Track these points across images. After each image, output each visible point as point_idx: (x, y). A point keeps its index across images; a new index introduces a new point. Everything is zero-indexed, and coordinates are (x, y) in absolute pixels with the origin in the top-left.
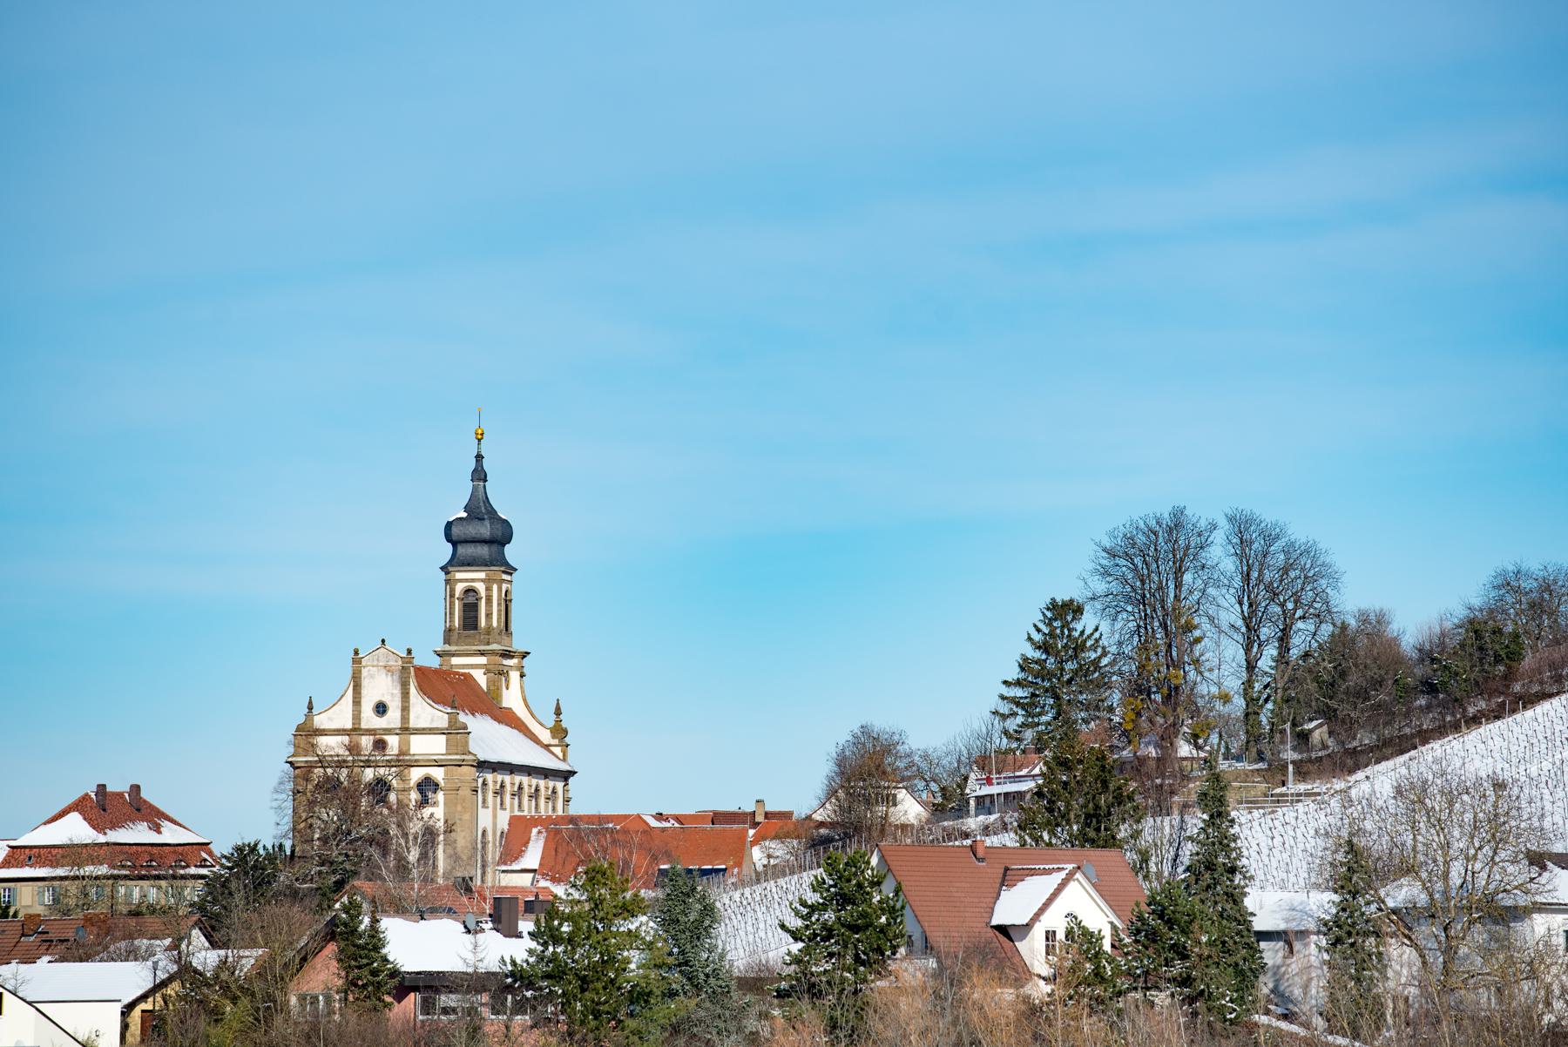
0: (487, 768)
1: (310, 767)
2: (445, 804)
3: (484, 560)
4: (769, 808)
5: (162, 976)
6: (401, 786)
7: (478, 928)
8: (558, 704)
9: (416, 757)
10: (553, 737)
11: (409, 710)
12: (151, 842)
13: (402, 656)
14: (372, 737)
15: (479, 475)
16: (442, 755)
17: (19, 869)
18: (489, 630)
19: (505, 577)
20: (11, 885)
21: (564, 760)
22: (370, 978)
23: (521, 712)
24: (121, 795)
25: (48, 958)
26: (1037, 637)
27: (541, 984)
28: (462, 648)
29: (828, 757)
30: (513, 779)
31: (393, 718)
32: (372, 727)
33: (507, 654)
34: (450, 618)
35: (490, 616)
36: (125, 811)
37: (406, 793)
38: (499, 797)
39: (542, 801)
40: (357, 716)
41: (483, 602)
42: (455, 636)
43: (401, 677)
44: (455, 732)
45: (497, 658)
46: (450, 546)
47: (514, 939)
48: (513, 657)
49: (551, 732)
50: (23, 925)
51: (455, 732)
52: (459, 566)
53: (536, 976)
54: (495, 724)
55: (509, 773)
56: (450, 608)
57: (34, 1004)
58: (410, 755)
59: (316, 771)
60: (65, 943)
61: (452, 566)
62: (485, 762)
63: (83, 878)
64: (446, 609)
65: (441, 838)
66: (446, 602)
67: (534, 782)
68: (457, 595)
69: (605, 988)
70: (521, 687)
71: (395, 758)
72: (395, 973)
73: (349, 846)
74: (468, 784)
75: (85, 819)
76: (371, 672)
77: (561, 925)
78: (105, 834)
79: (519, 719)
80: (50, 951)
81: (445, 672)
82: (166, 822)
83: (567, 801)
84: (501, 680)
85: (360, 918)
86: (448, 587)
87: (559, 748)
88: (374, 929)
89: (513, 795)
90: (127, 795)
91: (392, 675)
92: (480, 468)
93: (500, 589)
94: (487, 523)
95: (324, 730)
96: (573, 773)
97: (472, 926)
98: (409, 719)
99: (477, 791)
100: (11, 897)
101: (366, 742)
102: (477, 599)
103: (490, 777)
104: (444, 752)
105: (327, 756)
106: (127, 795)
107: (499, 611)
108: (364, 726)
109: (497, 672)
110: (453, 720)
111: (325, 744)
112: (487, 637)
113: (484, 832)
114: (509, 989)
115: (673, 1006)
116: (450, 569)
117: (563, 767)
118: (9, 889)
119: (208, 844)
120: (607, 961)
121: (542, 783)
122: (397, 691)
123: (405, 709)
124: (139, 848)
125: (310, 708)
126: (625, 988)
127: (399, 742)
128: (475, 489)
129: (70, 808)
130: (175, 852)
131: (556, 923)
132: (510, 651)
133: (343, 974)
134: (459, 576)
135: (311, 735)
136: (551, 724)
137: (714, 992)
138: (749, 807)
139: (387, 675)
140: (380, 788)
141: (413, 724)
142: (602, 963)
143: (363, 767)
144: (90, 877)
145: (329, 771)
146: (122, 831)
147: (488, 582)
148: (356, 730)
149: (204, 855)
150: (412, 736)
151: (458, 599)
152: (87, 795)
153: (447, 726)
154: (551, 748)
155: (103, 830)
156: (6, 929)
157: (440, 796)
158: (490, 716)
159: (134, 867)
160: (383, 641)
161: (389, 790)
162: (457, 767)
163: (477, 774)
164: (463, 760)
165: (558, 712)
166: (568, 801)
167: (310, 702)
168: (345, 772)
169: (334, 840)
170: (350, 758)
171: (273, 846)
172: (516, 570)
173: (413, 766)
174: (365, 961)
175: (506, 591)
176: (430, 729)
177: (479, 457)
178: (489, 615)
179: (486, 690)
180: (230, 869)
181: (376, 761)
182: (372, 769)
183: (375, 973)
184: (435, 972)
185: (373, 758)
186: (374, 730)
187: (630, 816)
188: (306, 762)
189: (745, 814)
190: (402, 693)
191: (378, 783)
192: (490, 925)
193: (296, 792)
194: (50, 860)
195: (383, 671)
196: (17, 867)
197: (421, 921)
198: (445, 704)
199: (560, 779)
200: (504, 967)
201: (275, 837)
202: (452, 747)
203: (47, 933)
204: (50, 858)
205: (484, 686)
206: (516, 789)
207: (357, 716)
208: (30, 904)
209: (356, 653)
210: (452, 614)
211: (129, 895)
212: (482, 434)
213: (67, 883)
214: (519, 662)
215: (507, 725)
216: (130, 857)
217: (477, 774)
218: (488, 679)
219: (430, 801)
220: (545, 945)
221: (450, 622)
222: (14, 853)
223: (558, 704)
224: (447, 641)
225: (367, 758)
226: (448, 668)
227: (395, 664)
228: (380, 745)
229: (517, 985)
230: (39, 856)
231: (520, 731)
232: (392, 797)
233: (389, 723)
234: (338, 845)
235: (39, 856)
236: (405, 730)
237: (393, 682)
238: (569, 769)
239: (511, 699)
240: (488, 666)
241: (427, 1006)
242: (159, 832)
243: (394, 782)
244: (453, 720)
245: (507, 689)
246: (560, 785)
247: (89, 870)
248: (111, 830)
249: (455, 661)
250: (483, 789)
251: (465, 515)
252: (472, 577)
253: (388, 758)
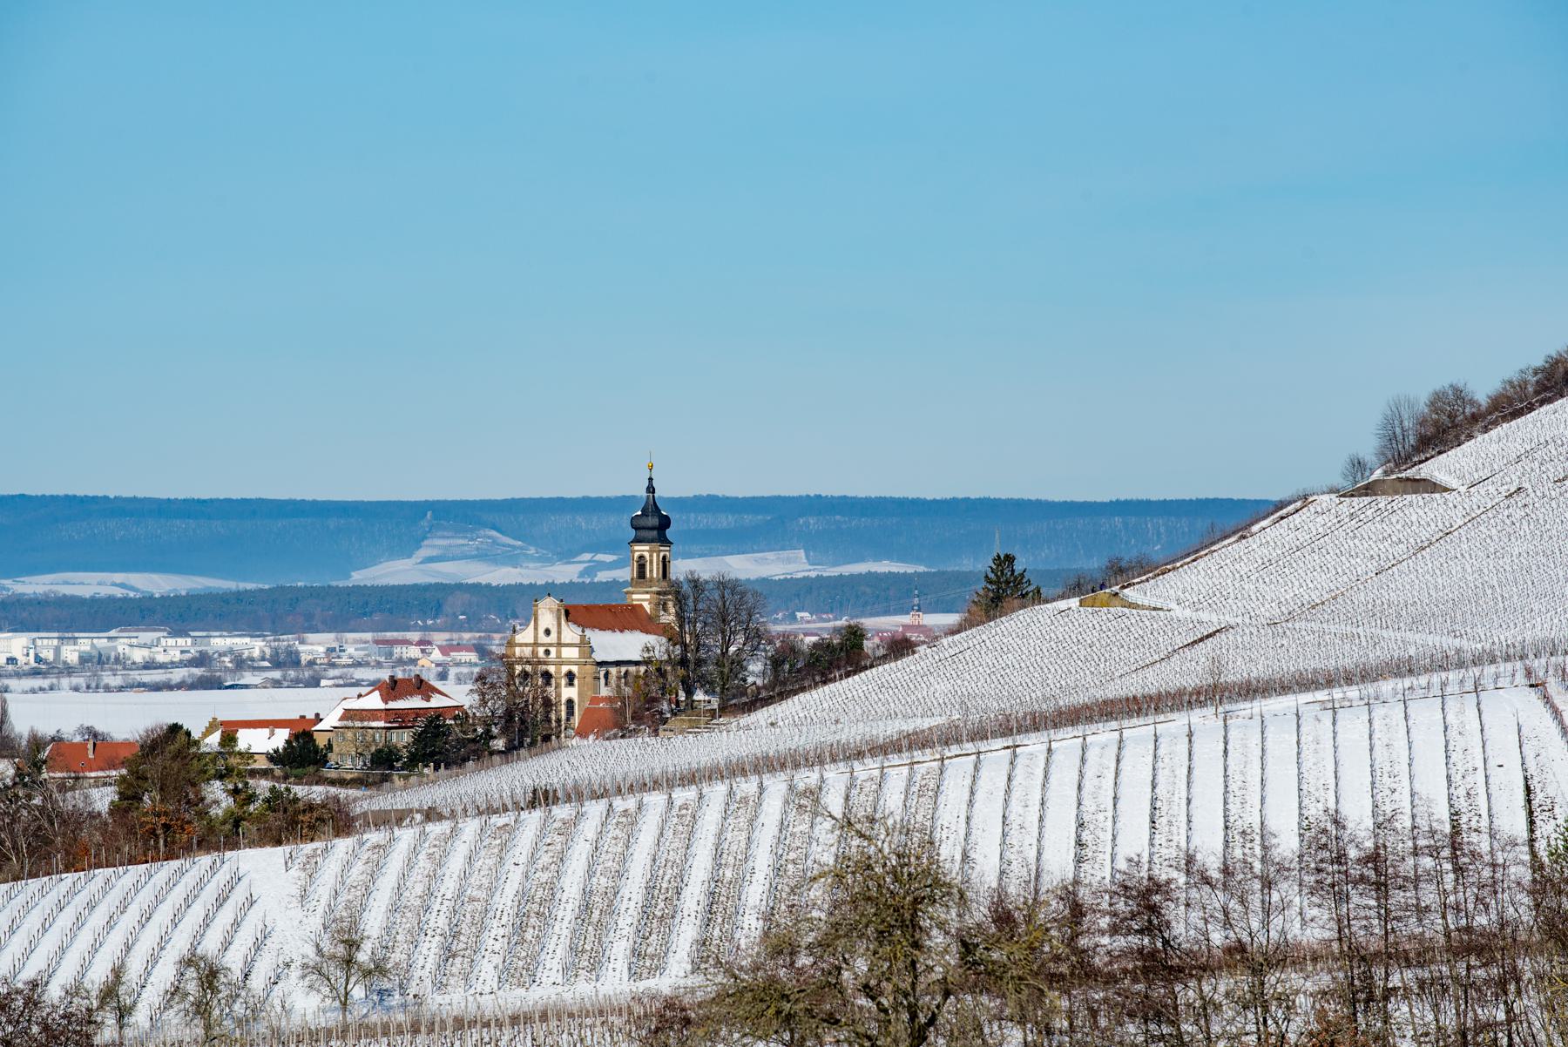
18: (652, 578)
26: (992, 576)
31: (553, 638)
40: (536, 637)
93: (658, 556)
101: (541, 651)
107: (658, 569)
122: (555, 623)
123: (559, 633)
134: (636, 548)
141: (563, 641)
147: (651, 552)
148: (536, 644)
159: (403, 721)
177: (651, 479)
178: (651, 571)
207: (536, 637)
228: (547, 652)
236: (560, 645)
249: (635, 596)
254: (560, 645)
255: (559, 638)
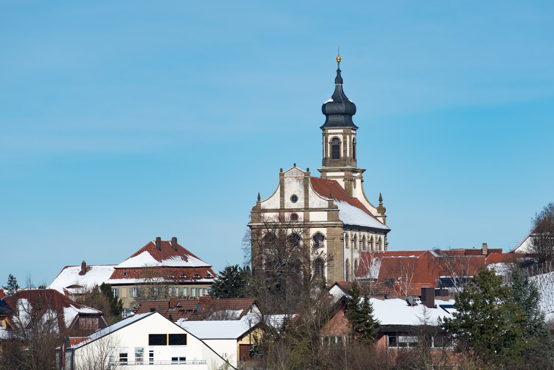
0: (348, 228)
1: (260, 228)
2: (327, 246)
3: (342, 123)
4: (490, 247)
5: (252, 325)
6: (306, 237)
7: (415, 303)
8: (381, 196)
9: (313, 223)
10: (379, 212)
11: (308, 199)
12: (183, 266)
13: (304, 172)
14: (291, 213)
15: (339, 80)
16: (326, 221)
17: (120, 279)
19: (353, 131)
20: (117, 287)
21: (384, 224)
22: (365, 328)
23: (362, 199)
24: (167, 242)
25: (183, 319)
27: (460, 330)
28: (332, 168)
29: (532, 220)
30: (369, 235)
31: (300, 203)
32: (291, 208)
33: (355, 171)
34: (326, 153)
35: (345, 151)
36: (170, 251)
37: (308, 241)
38: (354, 243)
39: (374, 244)
40: (282, 203)
41: (342, 144)
42: (328, 162)
43: (304, 183)
44: (332, 210)
45: (350, 173)
46: (325, 116)
47: (433, 309)
48: (357, 172)
49: (377, 210)
50: (169, 303)
51: (332, 210)
52: (330, 126)
53: (457, 326)
54: (350, 206)
55: (358, 230)
56: (325, 148)
57: (202, 340)
58: (310, 222)
59: (263, 230)
60: (190, 312)
61: (326, 126)
62: (347, 225)
63: (153, 283)
64: (323, 148)
65: (326, 264)
66: (323, 145)
67: (370, 235)
68: (329, 141)
69: (493, 333)
70: (362, 187)
71: (303, 223)
72: (377, 325)
73: (283, 268)
74: (339, 236)
75: (151, 254)
76: (289, 180)
77: (469, 301)
78: (161, 262)
79: (361, 203)
80: (183, 316)
81: (324, 180)
82: (190, 256)
83: (386, 244)
84: (352, 184)
85: (359, 298)
86: (324, 137)
87: (382, 218)
88: (366, 303)
89: (360, 241)
90: (170, 243)
91: (300, 182)
92: (339, 77)
94: (343, 104)
95: (267, 210)
96: (389, 230)
97: (411, 302)
98: (308, 204)
99: (343, 240)
100: (117, 293)
101: (287, 215)
102: (339, 143)
103: (349, 233)
104: (327, 220)
105: (269, 222)
106: (170, 243)
107: (350, 149)
108: (286, 207)
109: (350, 180)
110: (331, 204)
111: (268, 216)
112: (344, 162)
113: (347, 260)
114: (444, 333)
115: (526, 342)
116: (325, 128)
117: (384, 227)
118: (116, 290)
119: (211, 267)
120: (493, 319)
121: (374, 235)
122: (302, 190)
123: (307, 199)
124: (178, 269)
125: (259, 198)
126: (503, 332)
127: (304, 215)
128: (337, 87)
129: (144, 249)
130: (195, 271)
131: (466, 300)
132: (356, 169)
133: (351, 326)
134: (330, 131)
135: (260, 212)
136: (378, 206)
137: (539, 335)
138: (479, 247)
139: (297, 181)
140: (295, 238)
141: (310, 206)
142: (491, 320)
143: (286, 228)
144: (156, 283)
145: (270, 230)
146: (169, 260)
147: (344, 134)
148: (282, 210)
149: (209, 273)
150: (310, 212)
151: (329, 143)
152: (151, 242)
153: (328, 207)
154: (378, 218)
155: (160, 260)
156: (161, 305)
157: (325, 242)
158: (347, 202)
160: (295, 165)
161: (299, 239)
162: (333, 228)
163: (343, 231)
164: (336, 224)
165: (381, 199)
166: (387, 245)
167: (259, 196)
168: (277, 230)
169: (275, 264)
170: (280, 224)
171: (244, 268)
172: (358, 128)
173: (311, 227)
174: (362, 319)
175: (354, 139)
176: (319, 209)
177: (339, 71)
178: (345, 151)
179: (344, 189)
180: (224, 279)
181: (293, 225)
182: (292, 229)
183: (367, 325)
184: (396, 325)
185: (291, 223)
186: (292, 209)
187: (424, 251)
188: (258, 226)
189: (477, 250)
190: (305, 191)
191: (294, 236)
192: (420, 302)
193: (253, 241)
194: (135, 275)
195: (295, 180)
196: (119, 278)
197: (385, 300)
198: (325, 196)
199: (383, 233)
200: (440, 322)
201: (244, 263)
202: (331, 218)
203: (181, 307)
204: (135, 274)
205: (343, 187)
206: (362, 239)
207: (282, 203)
208: (126, 297)
209: (281, 170)
210: (326, 151)
211: (173, 292)
212: (340, 59)
213: (144, 286)
214: (361, 175)
215: (355, 206)
216: (175, 273)
217: (343, 231)
218: (345, 183)
219: (320, 245)
220: (461, 310)
221: (325, 154)
222: (117, 271)
223: (381, 196)
224: (324, 164)
225: (288, 223)
226: (325, 178)
227: (301, 176)
228: (294, 217)
229: (447, 331)
230: (130, 273)
231: (362, 209)
232: (301, 243)
233: (298, 206)
234: (276, 267)
235: (130, 273)
236: (307, 209)
237: (300, 185)
238: (387, 228)
239: (357, 193)
240: (345, 177)
241: (392, 342)
242: (187, 261)
243: (302, 236)
244: (331, 204)
245: (355, 188)
246: (383, 237)
247: (155, 280)
248: (164, 260)
249: (328, 174)
250: (346, 239)
251: (332, 100)
252: (336, 132)
253: (299, 223)
254: (307, 209)
255: (306, 203)
